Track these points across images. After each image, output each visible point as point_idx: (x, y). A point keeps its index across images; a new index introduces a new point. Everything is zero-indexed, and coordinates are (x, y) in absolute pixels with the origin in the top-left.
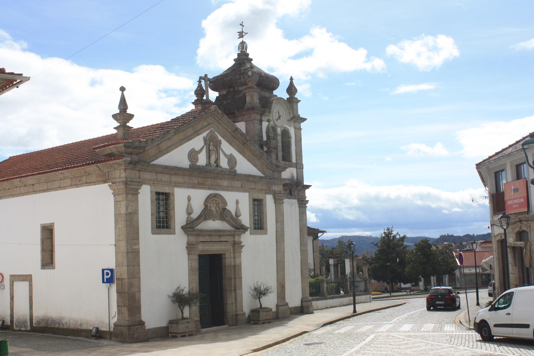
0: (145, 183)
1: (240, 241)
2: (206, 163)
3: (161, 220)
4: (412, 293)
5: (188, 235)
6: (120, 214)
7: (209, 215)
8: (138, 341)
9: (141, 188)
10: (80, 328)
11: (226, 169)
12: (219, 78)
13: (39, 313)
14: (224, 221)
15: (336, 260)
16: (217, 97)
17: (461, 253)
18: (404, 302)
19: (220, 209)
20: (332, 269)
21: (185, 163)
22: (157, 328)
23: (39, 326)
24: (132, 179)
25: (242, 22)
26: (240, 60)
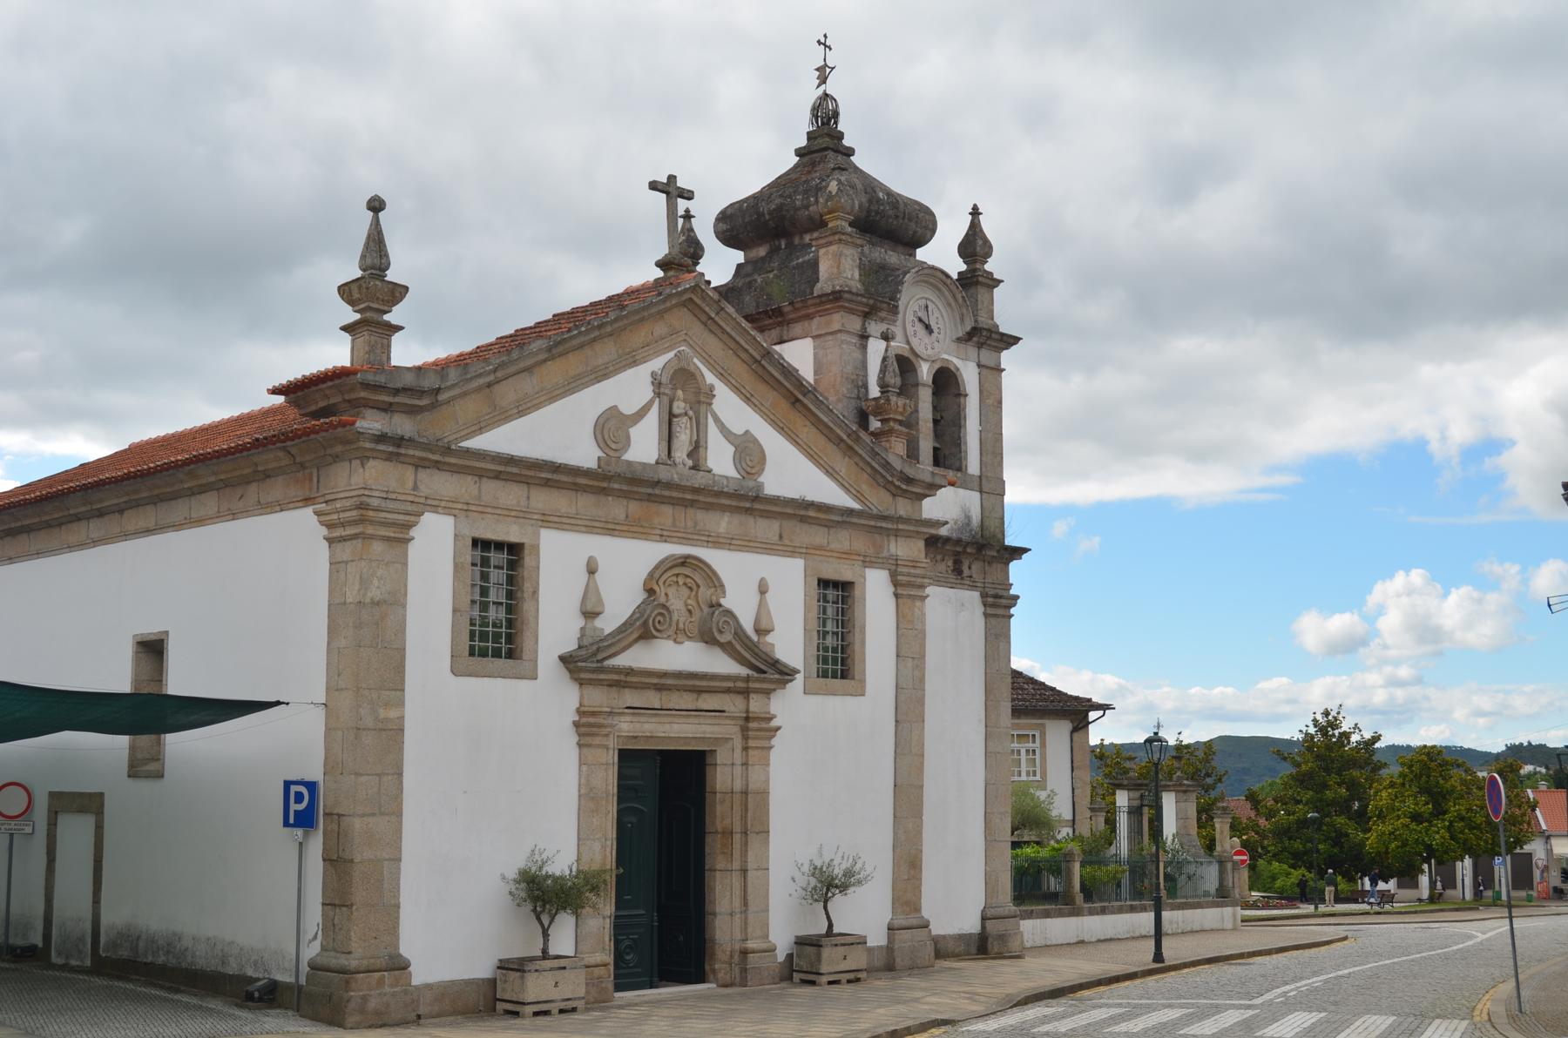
0: (435, 509)
1: (769, 713)
2: (657, 457)
3: (490, 629)
4: (1387, 907)
5: (581, 684)
6: (345, 603)
7: (659, 622)
8: (380, 1023)
9: (417, 523)
10: (220, 969)
11: (727, 478)
12: (745, 205)
13: (114, 916)
14: (714, 644)
15: (1137, 794)
16: (739, 266)
17: (1495, 777)
18: (1343, 935)
19: (701, 603)
20: (1123, 821)
21: (585, 455)
22: (453, 982)
23: (114, 957)
24: (387, 492)
25: (825, 36)
26: (813, 152)
